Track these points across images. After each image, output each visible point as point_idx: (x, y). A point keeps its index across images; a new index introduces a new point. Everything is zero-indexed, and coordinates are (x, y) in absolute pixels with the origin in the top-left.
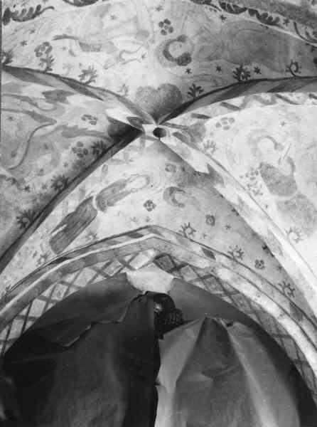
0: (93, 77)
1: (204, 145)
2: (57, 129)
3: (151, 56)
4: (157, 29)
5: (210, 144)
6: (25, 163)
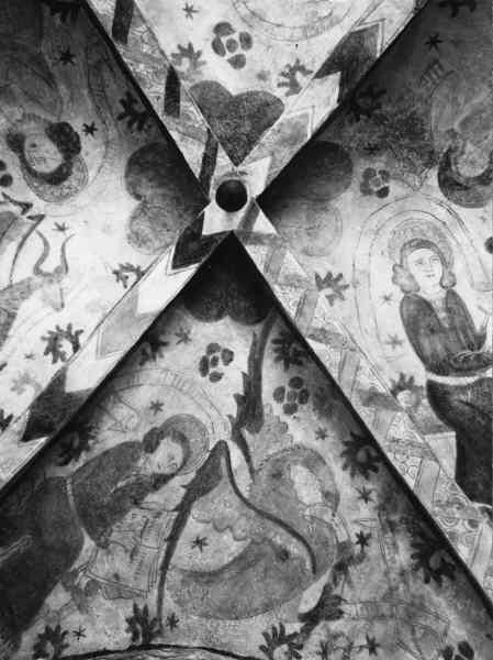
1: (287, 94)
5: (287, 80)
6: (303, 531)
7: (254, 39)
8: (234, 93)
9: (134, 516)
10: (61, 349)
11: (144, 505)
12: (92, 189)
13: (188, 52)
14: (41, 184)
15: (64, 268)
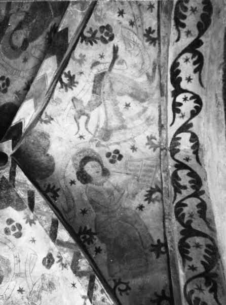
3: (83, 144)
4: (112, 149)
7: (3, 232)
10: (68, 78)
13: (31, 222)
15: (76, 119)
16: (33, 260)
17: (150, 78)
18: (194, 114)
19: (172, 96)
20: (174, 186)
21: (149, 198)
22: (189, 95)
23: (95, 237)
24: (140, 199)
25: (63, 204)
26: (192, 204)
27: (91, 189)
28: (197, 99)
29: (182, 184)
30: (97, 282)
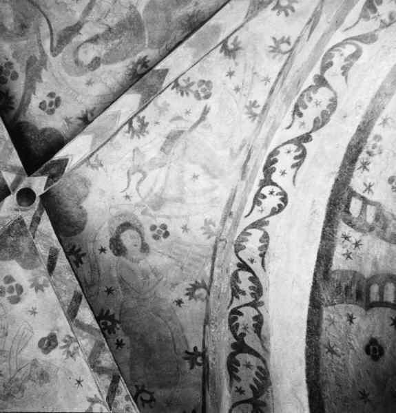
0: (134, 132)
2: (43, 53)
3: (126, 207)
4: (159, 222)
8: (14, 261)
9: (112, 21)
11: (105, 26)
12: (107, 217)
13: (38, 288)
14: (135, 224)
16: (26, 336)
17: (233, 155)
18: (276, 211)
19: (260, 184)
20: (232, 289)
21: (191, 293)
22: (277, 190)
23: (118, 326)
24: (179, 293)
25: (86, 275)
26: (249, 313)
27: (122, 265)
28: (284, 199)
29: (241, 288)
30: (122, 385)
